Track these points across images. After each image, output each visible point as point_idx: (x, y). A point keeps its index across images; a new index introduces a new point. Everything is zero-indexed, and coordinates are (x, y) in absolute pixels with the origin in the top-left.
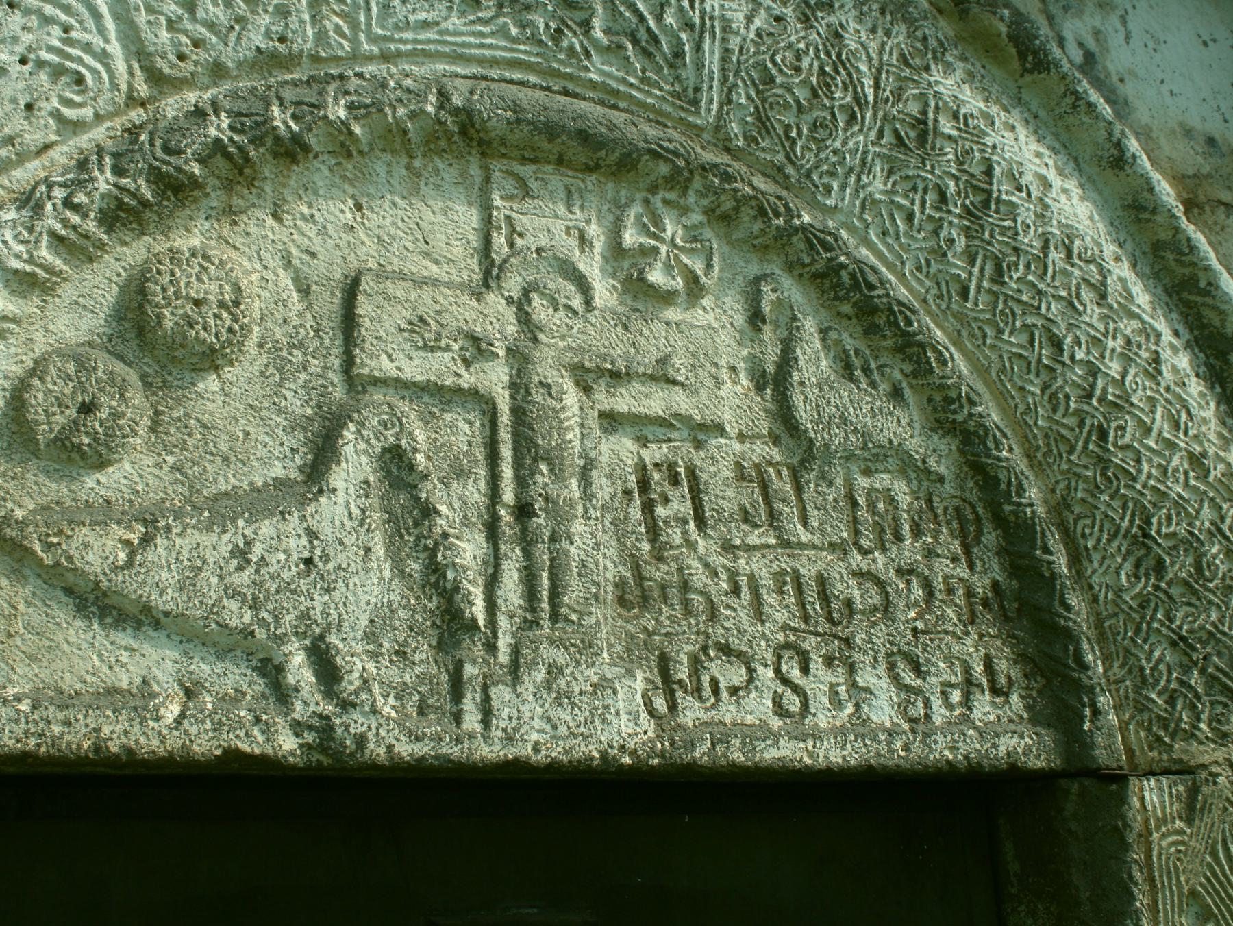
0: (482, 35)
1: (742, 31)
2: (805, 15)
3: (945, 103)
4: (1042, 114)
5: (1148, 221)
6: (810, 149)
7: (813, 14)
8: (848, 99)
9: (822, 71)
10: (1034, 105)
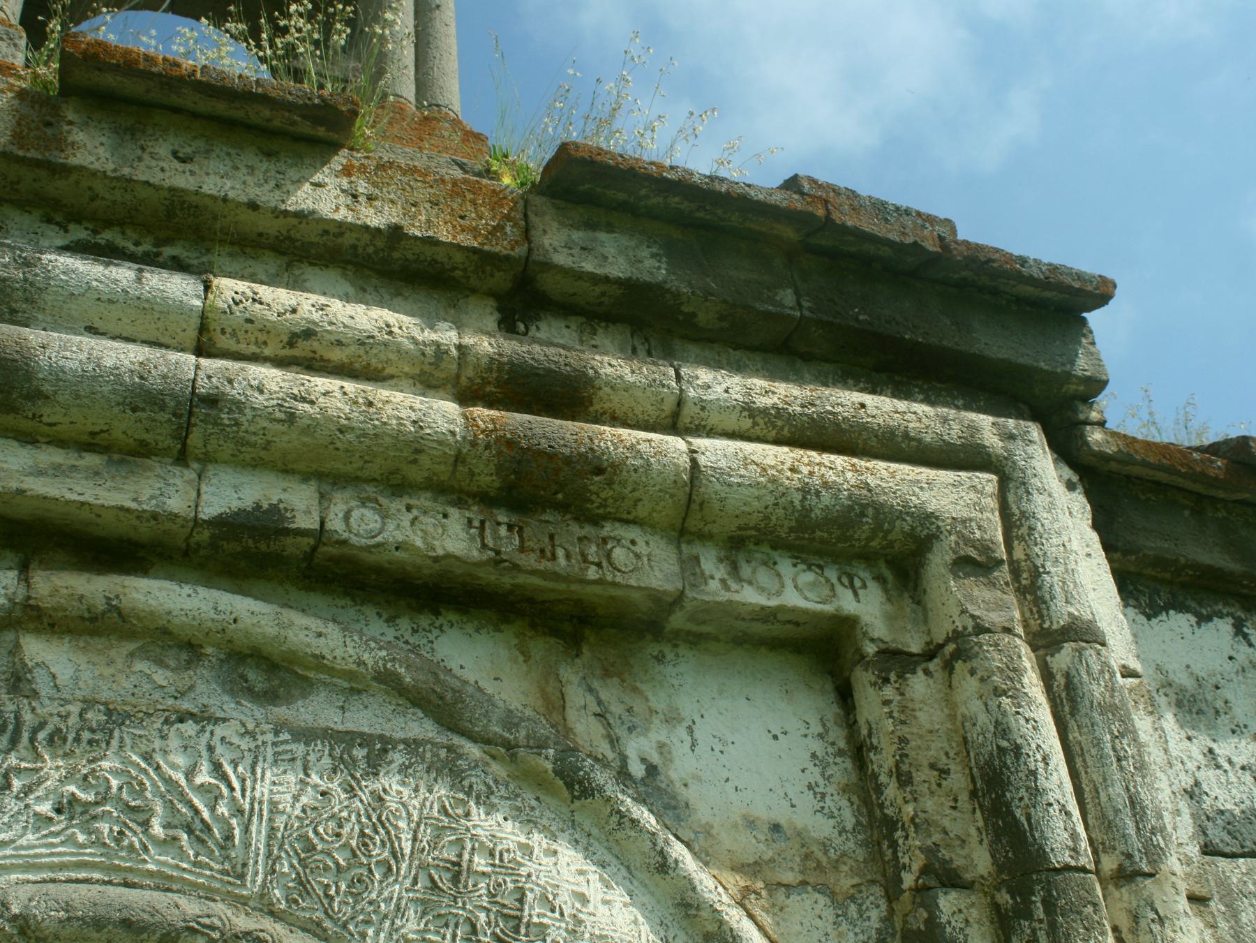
0: (53, 845)
1: (289, 809)
2: (351, 786)
3: (482, 843)
4: (595, 831)
5: (695, 916)
6: (347, 904)
7: (358, 783)
8: (386, 854)
9: (362, 834)
10: (587, 825)
